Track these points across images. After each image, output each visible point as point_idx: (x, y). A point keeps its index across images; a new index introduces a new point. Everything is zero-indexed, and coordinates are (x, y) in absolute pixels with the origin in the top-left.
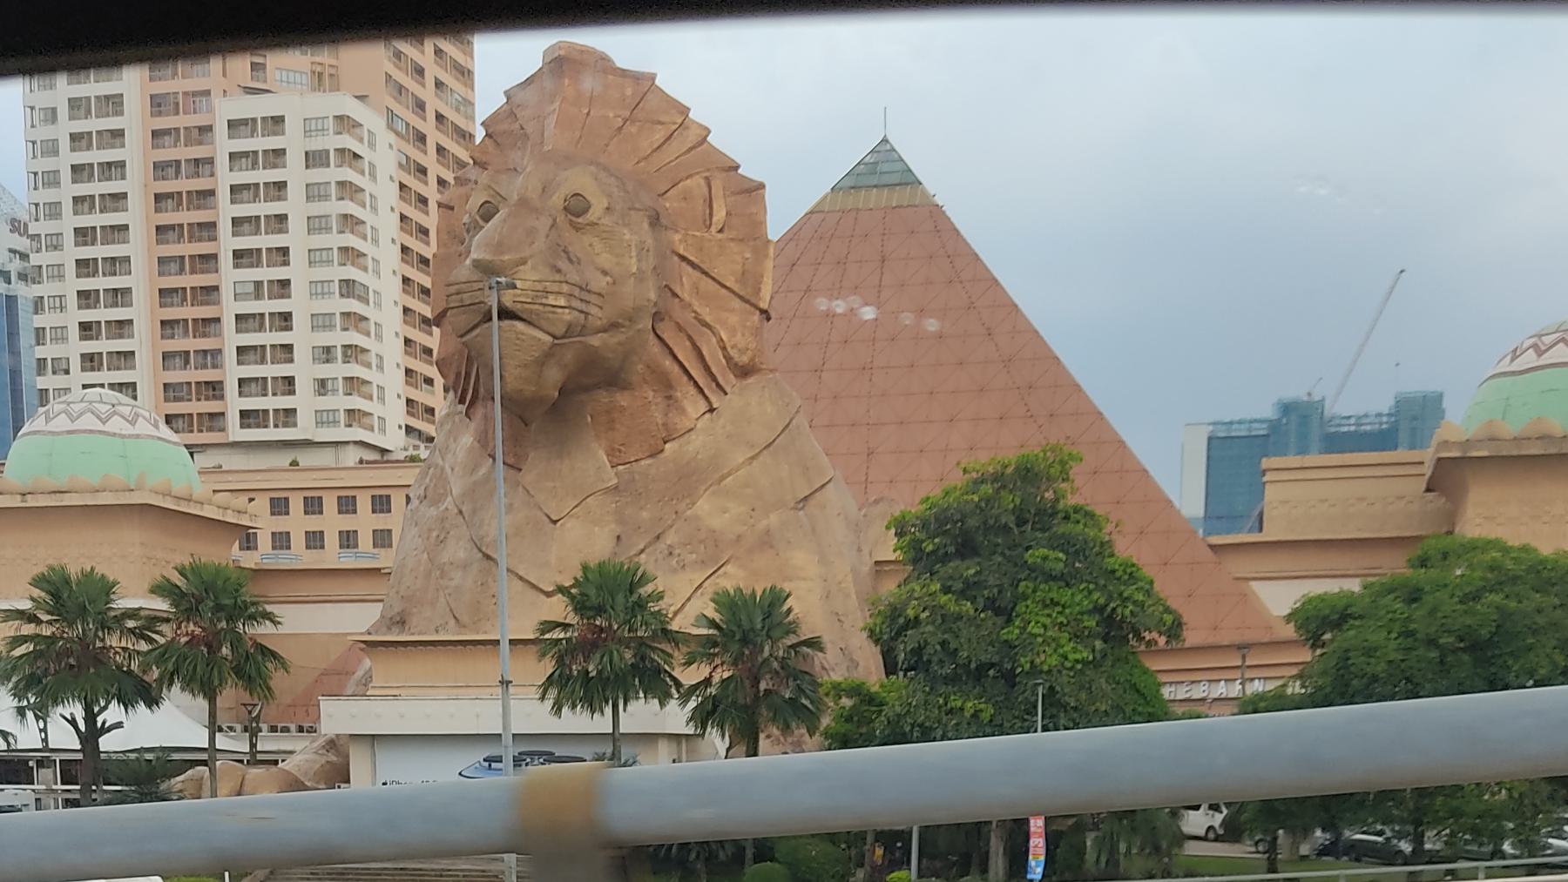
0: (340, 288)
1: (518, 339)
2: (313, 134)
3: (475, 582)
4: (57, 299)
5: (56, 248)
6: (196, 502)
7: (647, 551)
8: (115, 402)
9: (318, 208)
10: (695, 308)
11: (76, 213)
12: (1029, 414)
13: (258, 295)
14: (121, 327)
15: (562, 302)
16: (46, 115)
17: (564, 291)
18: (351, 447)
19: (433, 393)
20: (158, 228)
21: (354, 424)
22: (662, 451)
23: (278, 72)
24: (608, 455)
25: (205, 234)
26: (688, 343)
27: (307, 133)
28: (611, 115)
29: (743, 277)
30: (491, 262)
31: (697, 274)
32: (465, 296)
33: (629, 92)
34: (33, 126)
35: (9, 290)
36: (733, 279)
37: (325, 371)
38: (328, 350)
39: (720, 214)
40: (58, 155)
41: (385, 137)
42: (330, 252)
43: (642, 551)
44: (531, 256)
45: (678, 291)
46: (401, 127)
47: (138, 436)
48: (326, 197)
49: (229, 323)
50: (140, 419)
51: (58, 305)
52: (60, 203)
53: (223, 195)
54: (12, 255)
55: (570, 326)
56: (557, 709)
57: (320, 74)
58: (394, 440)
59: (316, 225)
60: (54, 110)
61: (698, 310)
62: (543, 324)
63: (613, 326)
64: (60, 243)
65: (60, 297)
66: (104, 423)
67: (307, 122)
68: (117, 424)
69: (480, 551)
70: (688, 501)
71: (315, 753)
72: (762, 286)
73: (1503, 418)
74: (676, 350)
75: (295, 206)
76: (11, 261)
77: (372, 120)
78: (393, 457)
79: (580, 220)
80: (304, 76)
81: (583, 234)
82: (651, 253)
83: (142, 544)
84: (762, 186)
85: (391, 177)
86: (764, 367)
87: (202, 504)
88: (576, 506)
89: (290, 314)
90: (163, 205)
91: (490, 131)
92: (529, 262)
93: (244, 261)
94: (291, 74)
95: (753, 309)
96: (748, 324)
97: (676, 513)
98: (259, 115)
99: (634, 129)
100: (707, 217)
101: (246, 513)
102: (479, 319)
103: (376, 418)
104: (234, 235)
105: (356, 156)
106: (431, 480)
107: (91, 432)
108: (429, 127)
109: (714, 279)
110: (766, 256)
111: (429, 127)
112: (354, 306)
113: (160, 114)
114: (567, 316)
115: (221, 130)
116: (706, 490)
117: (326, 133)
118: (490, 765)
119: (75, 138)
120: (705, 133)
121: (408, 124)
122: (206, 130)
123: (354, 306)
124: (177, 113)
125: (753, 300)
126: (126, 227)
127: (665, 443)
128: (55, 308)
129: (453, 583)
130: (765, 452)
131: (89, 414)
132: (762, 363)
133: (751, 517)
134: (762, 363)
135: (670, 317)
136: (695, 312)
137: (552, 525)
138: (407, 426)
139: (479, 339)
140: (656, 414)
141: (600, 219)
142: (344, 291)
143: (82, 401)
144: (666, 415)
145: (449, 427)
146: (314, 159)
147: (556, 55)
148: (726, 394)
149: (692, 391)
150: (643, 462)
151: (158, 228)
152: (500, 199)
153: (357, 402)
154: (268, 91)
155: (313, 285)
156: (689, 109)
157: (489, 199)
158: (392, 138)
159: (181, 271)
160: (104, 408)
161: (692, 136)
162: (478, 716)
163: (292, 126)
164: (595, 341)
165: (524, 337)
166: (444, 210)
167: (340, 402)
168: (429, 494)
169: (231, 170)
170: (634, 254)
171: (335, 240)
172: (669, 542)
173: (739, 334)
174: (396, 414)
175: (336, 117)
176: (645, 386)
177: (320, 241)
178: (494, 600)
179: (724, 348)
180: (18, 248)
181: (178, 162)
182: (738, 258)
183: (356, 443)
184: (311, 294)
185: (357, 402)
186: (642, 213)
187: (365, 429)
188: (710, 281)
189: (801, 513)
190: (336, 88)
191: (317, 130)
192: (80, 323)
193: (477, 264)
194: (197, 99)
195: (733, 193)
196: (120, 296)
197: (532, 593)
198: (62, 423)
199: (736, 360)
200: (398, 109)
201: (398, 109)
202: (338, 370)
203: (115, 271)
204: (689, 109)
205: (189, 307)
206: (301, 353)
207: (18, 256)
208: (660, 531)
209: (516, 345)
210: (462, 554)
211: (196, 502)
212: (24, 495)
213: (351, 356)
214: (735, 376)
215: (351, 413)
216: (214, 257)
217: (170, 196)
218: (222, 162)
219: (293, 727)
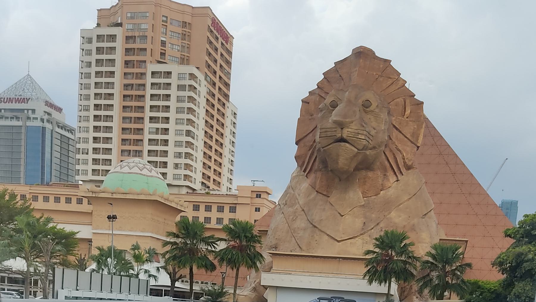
0: (186, 133)
1: (346, 149)
2: (181, 79)
3: (309, 235)
4: (86, 128)
5: (87, 110)
6: (170, 201)
7: (374, 228)
8: (144, 164)
9: (181, 105)
10: (396, 144)
11: (95, 99)
12: (462, 193)
13: (157, 133)
14: (108, 140)
15: (363, 138)
16: (87, 64)
17: (364, 134)
18: (184, 188)
19: (210, 172)
20: (124, 107)
21: (186, 180)
22: (379, 194)
23: (169, 57)
24: (362, 194)
25: (140, 110)
26: (393, 156)
27: (179, 78)
28: (375, 74)
29: (413, 135)
30: (342, 121)
31: (397, 132)
32: (328, 133)
33: (381, 66)
34: (82, 68)
35: (43, 125)
36: (409, 135)
37: (178, 161)
38: (180, 153)
39: (408, 112)
40: (90, 78)
41: (204, 82)
42: (184, 120)
43: (372, 228)
44: (355, 120)
45: (392, 138)
46: (208, 79)
47: (152, 176)
48: (184, 101)
49: (146, 142)
50: (153, 170)
51: (86, 130)
52: (90, 95)
53: (148, 97)
54: (45, 113)
55: (365, 145)
56: (370, 282)
57: (183, 59)
58: (198, 186)
59: (179, 110)
60: (91, 63)
61: (397, 145)
62: (356, 145)
63: (374, 148)
64: (89, 109)
65: (87, 127)
66: (141, 171)
67: (179, 74)
68: (145, 172)
69: (312, 224)
70: (388, 212)
71: (251, 291)
72: (419, 138)
73: (63, 269)
74: (389, 159)
75: (173, 103)
76: (44, 115)
77: (200, 76)
79: (368, 109)
80: (178, 59)
81: (368, 114)
82: (388, 123)
83: (151, 214)
84: (423, 103)
85: (205, 96)
86: (415, 167)
87: (171, 202)
88: (350, 211)
89: (168, 140)
90: (126, 99)
92: (354, 123)
93: (153, 121)
94: (174, 58)
95: (415, 146)
96: (413, 151)
97: (384, 216)
98: (163, 71)
99: (381, 79)
100: (403, 113)
101: (183, 206)
102: (332, 142)
103: (193, 179)
104: (150, 111)
105: (195, 88)
106: (288, 198)
107: (137, 173)
108: (217, 80)
109: (403, 134)
110: (422, 127)
111: (217, 80)
112: (190, 139)
113: (127, 67)
114: (365, 142)
115: (149, 75)
116: (394, 209)
117: (186, 79)
118: (320, 301)
119: (97, 73)
120: (405, 83)
121: (211, 79)
122: (143, 74)
123: (190, 139)
124: (134, 68)
125: (416, 143)
126: (113, 105)
127: (381, 191)
128: (85, 131)
129: (299, 235)
130: (413, 197)
131: (136, 167)
132: (414, 165)
133: (409, 220)
134: (414, 165)
135: (389, 146)
136: (396, 145)
137: (341, 217)
138: (202, 182)
139: (331, 148)
140: (380, 181)
142: (187, 134)
143: (133, 162)
144: (383, 181)
145: (297, 180)
146: (181, 88)
147: (359, 51)
148: (403, 175)
149: (392, 173)
150: (373, 197)
151: (124, 107)
152: (338, 99)
153: (188, 172)
154: (166, 63)
155: (177, 131)
156: (400, 74)
158: (206, 83)
159: (131, 122)
160: (141, 166)
161: (401, 83)
162: (320, 283)
163: (174, 76)
164: (368, 152)
165: (348, 149)
166: (305, 104)
167: (182, 172)
168: (288, 203)
169: (151, 89)
170: (383, 123)
171: (185, 116)
172: (381, 226)
173: (409, 155)
174: (199, 177)
175: (189, 74)
176: (378, 170)
177: (180, 116)
178: (316, 242)
179: (404, 159)
180: (47, 111)
181: (133, 85)
182: (412, 128)
183: (186, 186)
185: (188, 172)
186: (386, 109)
187: (190, 182)
188: (401, 135)
189: (424, 219)
190: (188, 64)
191: (182, 78)
192: (93, 137)
193: (335, 122)
194: (141, 63)
195: (413, 105)
196: (109, 129)
197: (332, 241)
198: (126, 169)
199: (408, 163)
200: (209, 73)
201: (209, 73)
202: (183, 161)
203: (107, 120)
204: (400, 74)
205: (132, 135)
206: (171, 154)
207: (47, 114)
208: (379, 222)
209: (345, 152)
210: (303, 225)
211: (170, 201)
212: (113, 193)
213: (187, 157)
214: (406, 169)
215: (186, 176)
216: (143, 118)
217: (129, 96)
218: (148, 86)
219: (200, 282)
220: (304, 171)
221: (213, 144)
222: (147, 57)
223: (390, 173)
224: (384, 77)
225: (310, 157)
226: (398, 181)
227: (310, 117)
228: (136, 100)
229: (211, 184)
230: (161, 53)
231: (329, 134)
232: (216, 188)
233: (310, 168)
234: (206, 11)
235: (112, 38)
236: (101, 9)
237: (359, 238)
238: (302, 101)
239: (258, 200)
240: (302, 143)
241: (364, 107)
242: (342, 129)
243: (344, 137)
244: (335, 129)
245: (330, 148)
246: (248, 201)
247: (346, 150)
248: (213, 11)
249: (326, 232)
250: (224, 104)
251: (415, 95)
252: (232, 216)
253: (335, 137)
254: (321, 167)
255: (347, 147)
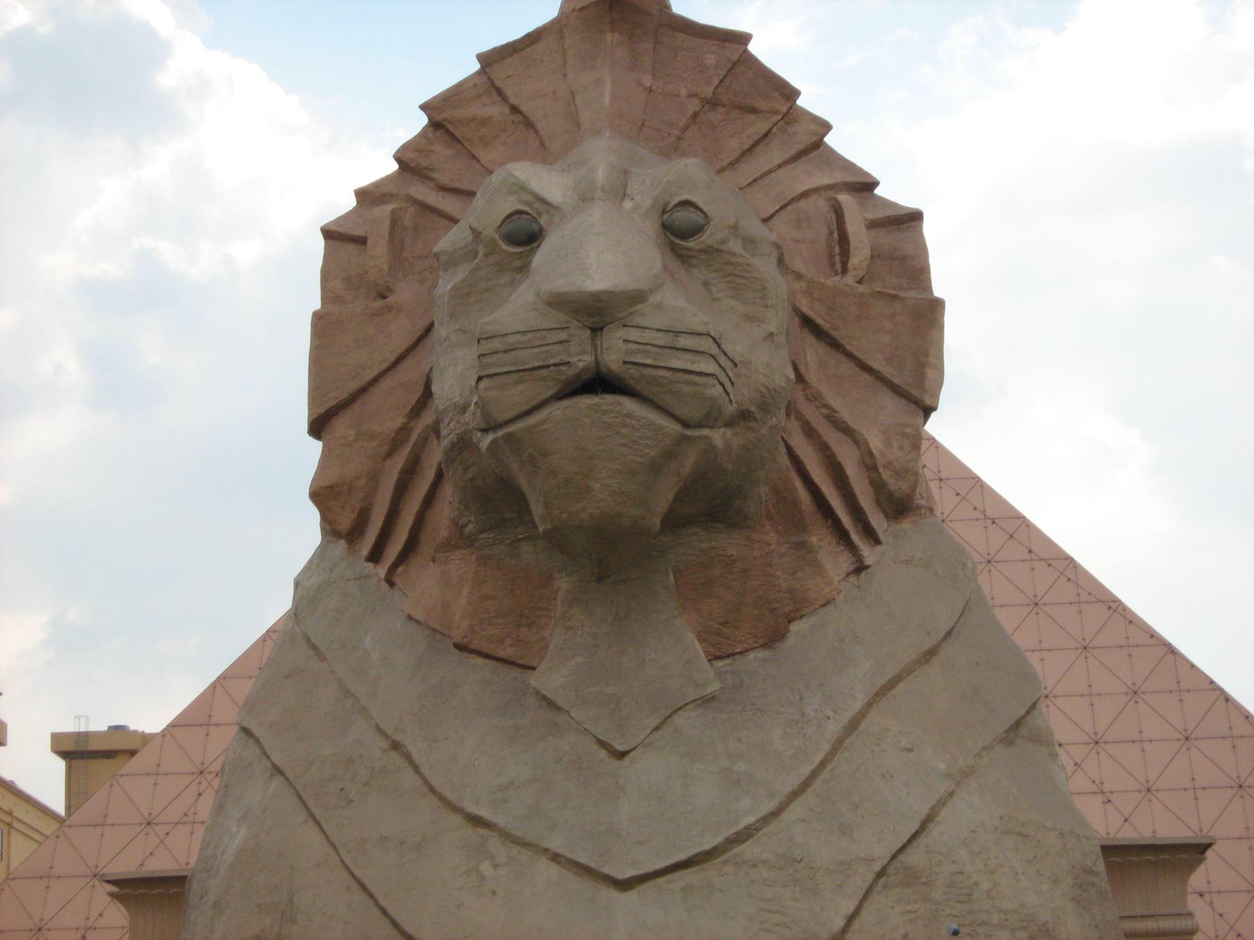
1: (625, 426)
63: (744, 416)
73: (1012, 634)
79: (691, 244)
88: (656, 729)
102: (551, 392)
125: (915, 392)
127: (790, 621)
136: (826, 406)
140: (779, 573)
141: (724, 242)
150: (752, 655)
157: (524, 208)
164: (718, 437)
220: (375, 556)
223: (820, 539)
224: (724, 106)
225: (402, 489)
226: (863, 574)
227: (379, 303)
231: (529, 358)
237: (721, 859)
238: (329, 234)
240: (341, 427)
242: (596, 330)
244: (563, 336)
245: (543, 422)
247: (623, 431)
249: (545, 844)
253: (563, 368)
254: (471, 526)
255: (629, 415)
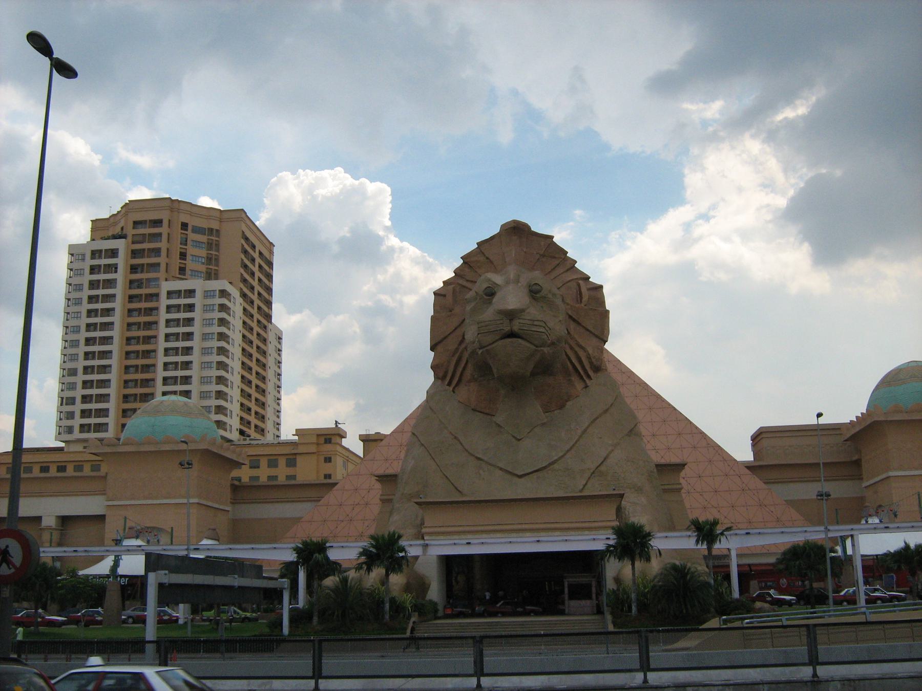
41: (239, 300)
57: (211, 244)
58: (235, 436)
63: (553, 344)
77: (235, 292)
78: (235, 443)
79: (537, 295)
91: (466, 261)
148: (591, 379)
150: (556, 412)
163: (199, 294)
164: (546, 350)
184: (202, 368)
190: (217, 278)
220: (449, 384)
221: (253, 378)
222: (162, 274)
223: (574, 378)
226: (587, 388)
227: (449, 313)
228: (145, 329)
229: (251, 432)
230: (180, 252)
232: (258, 436)
233: (457, 379)
234: (239, 216)
235: (113, 253)
236: (97, 220)
238: (435, 293)
239: (328, 447)
240: (439, 348)
241: (533, 292)
243: (516, 330)
244: (501, 321)
246: (313, 449)
248: (248, 214)
249: (498, 465)
250: (265, 327)
251: (590, 278)
252: (290, 471)
